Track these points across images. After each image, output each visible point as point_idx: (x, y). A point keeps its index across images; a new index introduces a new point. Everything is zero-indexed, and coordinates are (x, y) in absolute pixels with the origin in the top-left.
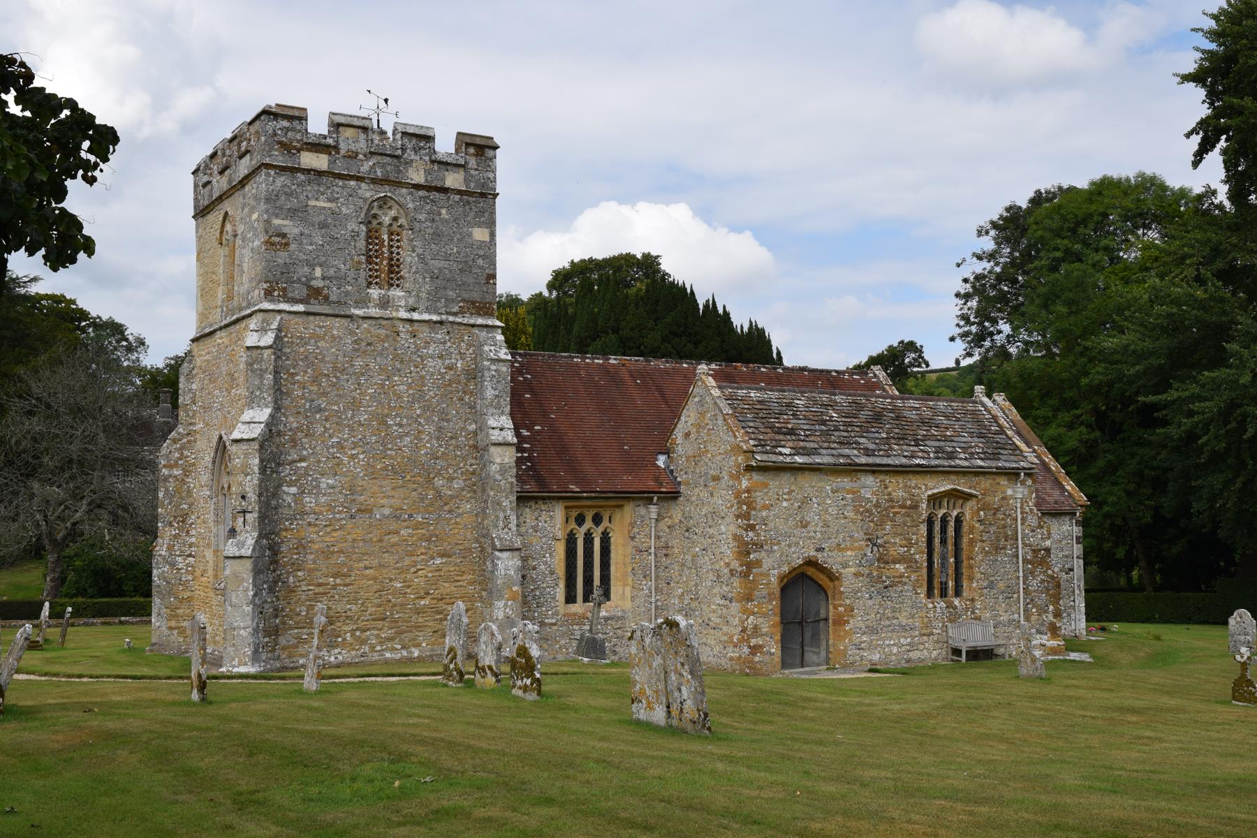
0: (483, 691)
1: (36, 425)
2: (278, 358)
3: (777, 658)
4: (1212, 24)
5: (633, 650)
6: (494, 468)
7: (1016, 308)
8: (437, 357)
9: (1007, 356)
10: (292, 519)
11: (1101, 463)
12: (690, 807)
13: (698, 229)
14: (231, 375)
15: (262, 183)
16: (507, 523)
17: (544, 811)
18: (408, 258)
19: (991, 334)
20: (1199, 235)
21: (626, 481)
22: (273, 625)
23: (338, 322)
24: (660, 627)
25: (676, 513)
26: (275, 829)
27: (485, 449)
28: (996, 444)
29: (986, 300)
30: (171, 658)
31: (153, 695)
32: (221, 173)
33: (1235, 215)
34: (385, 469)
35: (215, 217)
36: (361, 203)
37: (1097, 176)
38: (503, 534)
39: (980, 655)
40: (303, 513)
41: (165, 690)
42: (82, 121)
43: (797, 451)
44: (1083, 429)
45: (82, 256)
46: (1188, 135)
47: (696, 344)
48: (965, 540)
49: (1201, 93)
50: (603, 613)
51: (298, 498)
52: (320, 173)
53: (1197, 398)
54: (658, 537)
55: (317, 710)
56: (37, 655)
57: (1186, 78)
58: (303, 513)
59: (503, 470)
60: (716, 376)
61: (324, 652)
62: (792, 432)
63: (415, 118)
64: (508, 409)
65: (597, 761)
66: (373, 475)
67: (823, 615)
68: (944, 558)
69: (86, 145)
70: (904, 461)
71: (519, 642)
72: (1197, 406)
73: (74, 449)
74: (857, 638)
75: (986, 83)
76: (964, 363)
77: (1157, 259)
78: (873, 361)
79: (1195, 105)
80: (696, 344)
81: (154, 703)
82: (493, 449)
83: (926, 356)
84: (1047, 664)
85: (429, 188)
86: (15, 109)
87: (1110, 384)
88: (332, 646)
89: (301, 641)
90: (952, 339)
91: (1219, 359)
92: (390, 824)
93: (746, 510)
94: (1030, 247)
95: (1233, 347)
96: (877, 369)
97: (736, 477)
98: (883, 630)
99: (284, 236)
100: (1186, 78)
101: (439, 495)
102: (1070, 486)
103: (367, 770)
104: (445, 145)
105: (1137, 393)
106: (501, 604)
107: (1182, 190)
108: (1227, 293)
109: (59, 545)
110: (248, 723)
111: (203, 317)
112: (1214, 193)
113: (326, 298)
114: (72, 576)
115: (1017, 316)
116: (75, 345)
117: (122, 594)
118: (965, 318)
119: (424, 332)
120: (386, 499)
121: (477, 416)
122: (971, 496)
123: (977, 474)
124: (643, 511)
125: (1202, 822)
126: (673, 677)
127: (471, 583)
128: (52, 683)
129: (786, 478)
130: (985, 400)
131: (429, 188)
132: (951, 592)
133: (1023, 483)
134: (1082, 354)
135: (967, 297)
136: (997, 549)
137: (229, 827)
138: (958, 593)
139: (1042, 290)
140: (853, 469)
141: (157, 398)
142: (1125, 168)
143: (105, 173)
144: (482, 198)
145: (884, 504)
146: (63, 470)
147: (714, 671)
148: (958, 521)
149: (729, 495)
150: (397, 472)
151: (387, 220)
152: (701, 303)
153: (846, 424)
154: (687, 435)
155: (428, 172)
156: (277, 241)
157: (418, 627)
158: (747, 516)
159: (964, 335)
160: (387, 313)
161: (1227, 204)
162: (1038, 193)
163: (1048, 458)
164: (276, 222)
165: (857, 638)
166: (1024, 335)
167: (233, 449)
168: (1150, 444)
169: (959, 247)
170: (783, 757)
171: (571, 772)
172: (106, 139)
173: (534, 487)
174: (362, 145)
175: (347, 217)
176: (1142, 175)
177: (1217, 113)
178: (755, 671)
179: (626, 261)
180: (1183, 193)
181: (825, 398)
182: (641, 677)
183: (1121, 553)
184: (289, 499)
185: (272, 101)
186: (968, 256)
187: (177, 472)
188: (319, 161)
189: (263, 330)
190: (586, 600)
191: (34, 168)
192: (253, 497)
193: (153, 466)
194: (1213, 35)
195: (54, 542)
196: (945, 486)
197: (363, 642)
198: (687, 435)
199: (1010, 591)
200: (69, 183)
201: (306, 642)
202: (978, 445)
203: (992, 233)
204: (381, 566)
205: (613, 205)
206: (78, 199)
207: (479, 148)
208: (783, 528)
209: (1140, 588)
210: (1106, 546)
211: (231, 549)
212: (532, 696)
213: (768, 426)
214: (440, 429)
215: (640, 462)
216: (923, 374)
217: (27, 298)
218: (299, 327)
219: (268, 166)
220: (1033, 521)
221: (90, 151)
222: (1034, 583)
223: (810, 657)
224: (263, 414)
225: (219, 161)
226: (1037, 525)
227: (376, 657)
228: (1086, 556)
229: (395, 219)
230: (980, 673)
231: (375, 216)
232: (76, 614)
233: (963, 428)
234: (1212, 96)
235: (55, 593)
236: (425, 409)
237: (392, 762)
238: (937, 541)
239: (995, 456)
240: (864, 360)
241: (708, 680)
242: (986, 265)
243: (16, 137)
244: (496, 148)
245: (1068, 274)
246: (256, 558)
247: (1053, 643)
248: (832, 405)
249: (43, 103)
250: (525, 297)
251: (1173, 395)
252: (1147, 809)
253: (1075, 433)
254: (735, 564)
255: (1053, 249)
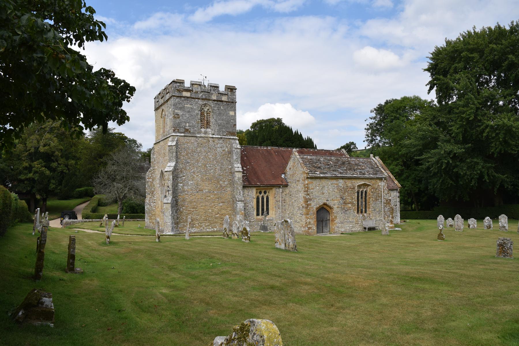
0: (234, 240)
1: (115, 168)
2: (177, 148)
3: (316, 231)
4: (431, 56)
5: (276, 229)
6: (236, 178)
7: (381, 133)
8: (220, 148)
9: (379, 146)
10: (181, 193)
11: (405, 176)
12: (291, 271)
13: (293, 111)
14: (164, 153)
15: (172, 101)
16: (240, 193)
17: (251, 272)
18: (212, 120)
19: (375, 140)
20: (430, 112)
21: (273, 182)
22: (177, 222)
23: (193, 138)
24: (283, 222)
25: (287, 190)
26: (179, 275)
27: (234, 173)
28: (376, 171)
29: (374, 130)
30: (151, 230)
31: (146, 240)
32: (162, 98)
33: (439, 107)
34: (206, 179)
35: (160, 110)
36: (199, 105)
37: (403, 96)
38: (239, 197)
39: (371, 229)
40: (184, 191)
41: (149, 239)
42: (127, 86)
43: (321, 173)
44: (400, 166)
45: (126, 121)
46: (426, 85)
47: (292, 143)
48: (368, 197)
49: (429, 74)
50: (267, 219)
51: (183, 187)
52: (188, 97)
53: (430, 158)
54: (282, 197)
55: (189, 244)
56: (117, 228)
57: (425, 70)
58: (184, 191)
59: (239, 179)
60: (298, 152)
61: (191, 229)
62: (319, 168)
63: (214, 82)
64: (240, 162)
65: (266, 259)
66: (203, 181)
67: (328, 218)
68: (362, 202)
69: (127, 92)
70: (351, 175)
71: (244, 226)
72: (430, 160)
73: (124, 174)
74: (337, 225)
75: (372, 70)
76: (367, 148)
77: (419, 119)
78: (342, 147)
79: (428, 77)
80: (292, 143)
81: (147, 242)
82: (236, 173)
83: (357, 146)
84: (389, 231)
85: (217, 101)
86: (110, 84)
87: (407, 154)
88: (193, 227)
89: (184, 226)
90: (364, 141)
91: (436, 147)
92: (210, 275)
93: (307, 189)
94: (385, 115)
95: (439, 143)
96: (343, 150)
97: (304, 180)
98: (345, 223)
99: (178, 115)
100: (425, 70)
101: (221, 186)
102: (396, 182)
103: (203, 261)
104: (222, 89)
105: (414, 156)
106: (238, 216)
107: (425, 100)
108: (437, 128)
109: (121, 200)
110: (171, 248)
111: (157, 137)
112: (434, 101)
113: (190, 132)
114: (125, 208)
115: (381, 134)
116: (124, 146)
117: (137, 213)
118: (367, 135)
119: (216, 141)
120: (206, 187)
121: (232, 164)
122: (369, 185)
123: (371, 179)
124: (278, 190)
125: (429, 272)
126: (287, 236)
127: (230, 210)
128: (121, 236)
129: (318, 180)
130: (373, 158)
131: (217, 101)
132: (364, 212)
133: (384, 181)
134: (399, 145)
135: (368, 129)
136: (376, 200)
137: (168, 275)
138: (365, 212)
139: (388, 128)
140: (337, 178)
141: (145, 160)
142: (410, 94)
143: (132, 99)
144: (232, 103)
145: (345, 188)
146: (121, 180)
147: (298, 234)
148: (366, 192)
149: (302, 186)
150: (209, 180)
151: (206, 110)
152: (294, 131)
153: (335, 165)
154: (290, 169)
155: (217, 96)
156: (176, 116)
157: (216, 222)
158: (307, 191)
159: (368, 140)
160: (206, 136)
161: (437, 104)
162: (387, 101)
163: (390, 174)
164: (176, 111)
165: (337, 225)
166: (384, 140)
167: (165, 174)
168: (417, 170)
169: (366, 116)
170: (317, 257)
171: (258, 262)
172: (132, 90)
173: (247, 184)
174: (199, 89)
175: (195, 109)
176: (415, 96)
177: (434, 80)
178: (310, 234)
179: (272, 120)
180: (425, 101)
181: (329, 158)
182: (278, 236)
183: (410, 200)
184: (180, 187)
185: (175, 78)
186: (368, 118)
187: (151, 180)
188: (188, 94)
189: (173, 141)
190: (262, 215)
191: (115, 98)
192: (170, 187)
193: (144, 178)
194: (432, 59)
195: (120, 199)
196: (362, 182)
197: (201, 226)
198: (290, 169)
199: (380, 211)
200: (123, 102)
201: (185, 226)
202: (371, 171)
203: (375, 112)
204: (206, 205)
205: (269, 104)
206: (125, 106)
207: (232, 89)
208: (317, 195)
209: (415, 210)
210: (406, 198)
211: (165, 201)
212: (248, 241)
213: (313, 166)
214: (221, 168)
215: (278, 177)
216: (356, 151)
217: (112, 134)
218: (182, 140)
219: (174, 96)
220: (386, 192)
221: (128, 93)
222: (386, 209)
223: (325, 230)
224: (173, 164)
225: (161, 95)
226: (387, 193)
227: (205, 230)
228: (400, 201)
229: (208, 109)
230: (371, 234)
231: (203, 109)
232: (126, 218)
233: (367, 166)
234: (432, 75)
235: (121, 212)
236: (217, 162)
237: (210, 259)
238: (360, 198)
239: (376, 174)
240: (340, 147)
241: (296, 237)
242: (373, 121)
243: (111, 91)
244: (236, 89)
245: (395, 123)
246: (172, 203)
247: (391, 225)
248: (331, 160)
249: (117, 81)
250: (244, 131)
251: (423, 157)
252: (415, 269)
253: (398, 167)
254: (304, 205)
255: (391, 116)
